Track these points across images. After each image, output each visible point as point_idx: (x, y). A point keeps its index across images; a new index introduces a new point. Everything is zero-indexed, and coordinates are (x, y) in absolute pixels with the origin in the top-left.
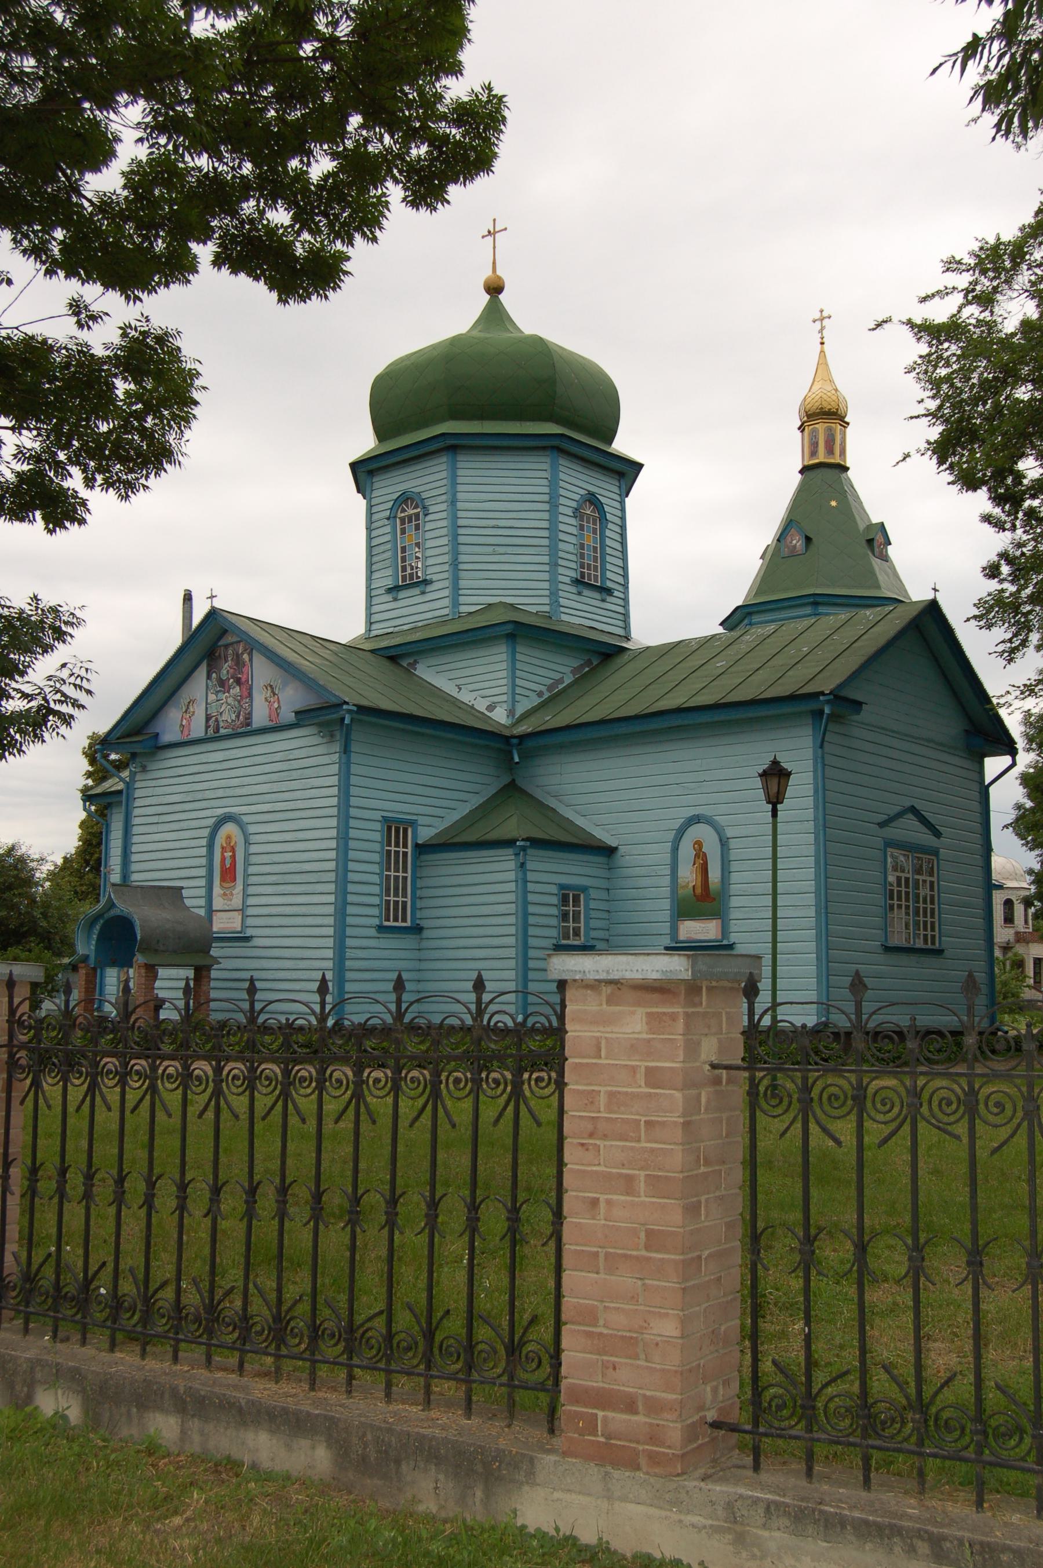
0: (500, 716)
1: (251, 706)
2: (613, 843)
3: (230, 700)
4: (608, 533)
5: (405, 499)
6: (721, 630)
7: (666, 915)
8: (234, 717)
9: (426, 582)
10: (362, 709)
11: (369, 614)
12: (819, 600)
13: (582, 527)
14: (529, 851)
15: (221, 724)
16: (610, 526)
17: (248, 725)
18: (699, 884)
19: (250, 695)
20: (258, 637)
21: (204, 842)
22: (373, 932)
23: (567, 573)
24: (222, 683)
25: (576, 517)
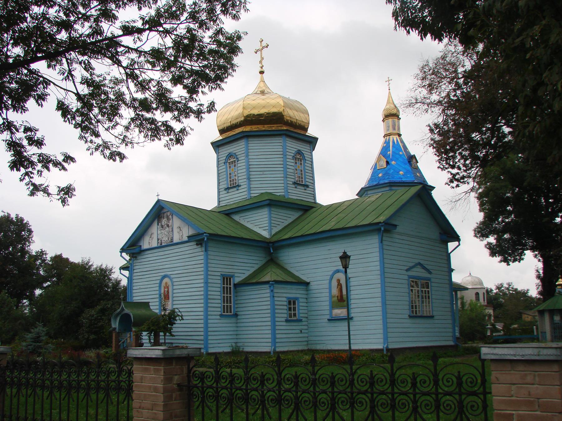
0: (265, 234)
1: (173, 234)
2: (308, 281)
3: (166, 233)
5: (230, 156)
6: (357, 197)
7: (328, 308)
9: (239, 186)
10: (211, 235)
11: (219, 198)
12: (391, 184)
13: (296, 163)
14: (275, 285)
15: (163, 242)
17: (172, 242)
18: (339, 295)
19: (172, 231)
21: (158, 285)
22: (218, 317)
23: (291, 181)
24: (162, 226)
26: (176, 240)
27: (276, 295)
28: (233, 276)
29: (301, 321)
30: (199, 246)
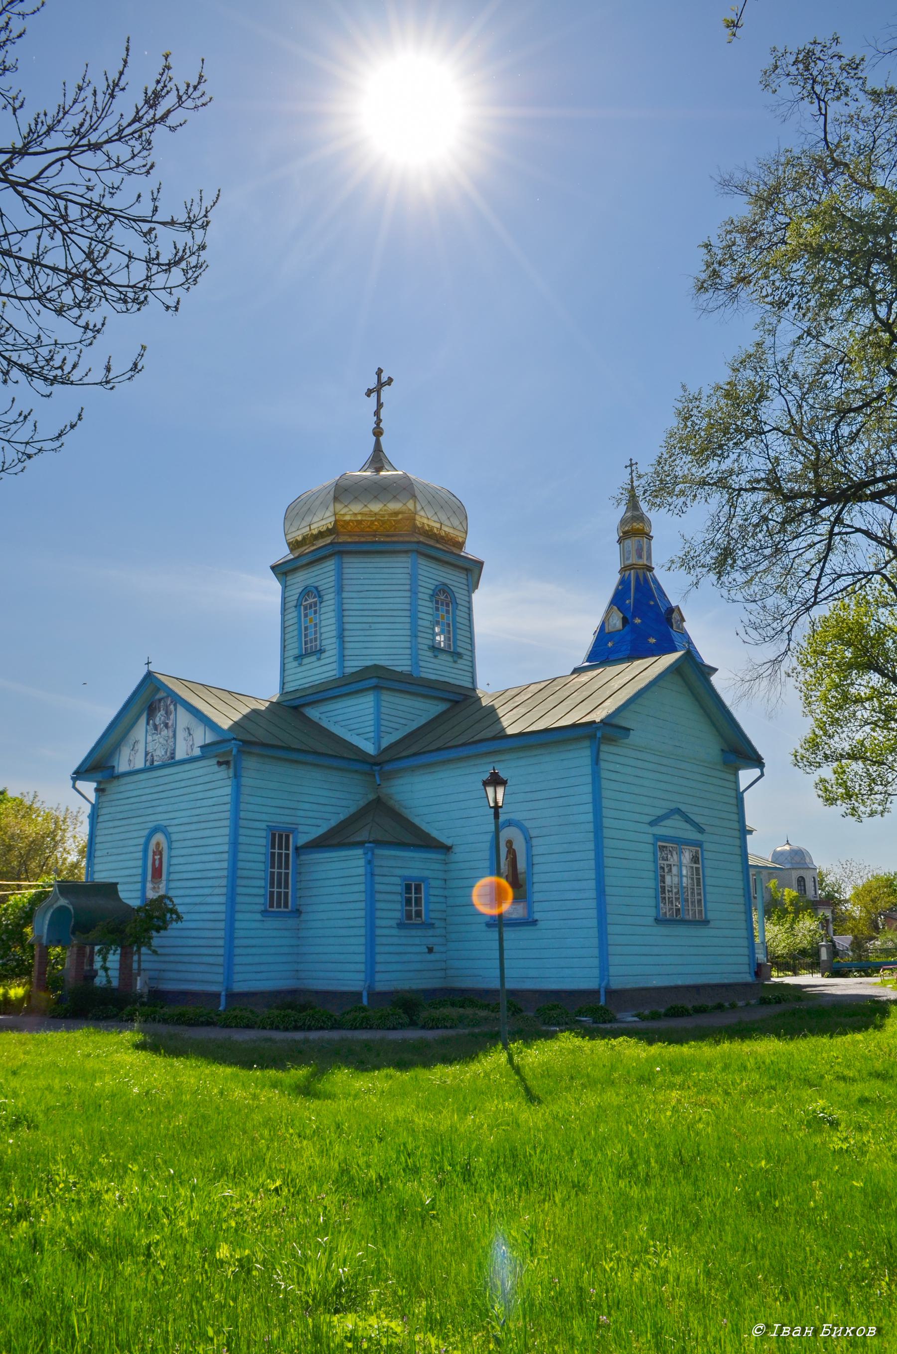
0: (369, 748)
1: (175, 744)
2: (448, 842)
3: (161, 740)
4: (458, 612)
5: (307, 592)
8: (163, 753)
13: (437, 609)
14: (378, 852)
15: (155, 758)
16: (460, 607)
17: (173, 758)
20: (180, 693)
22: (258, 917)
24: (156, 727)
25: (432, 601)
26: (180, 755)
27: (377, 871)
28: (293, 831)
29: (431, 926)
30: (224, 767)
